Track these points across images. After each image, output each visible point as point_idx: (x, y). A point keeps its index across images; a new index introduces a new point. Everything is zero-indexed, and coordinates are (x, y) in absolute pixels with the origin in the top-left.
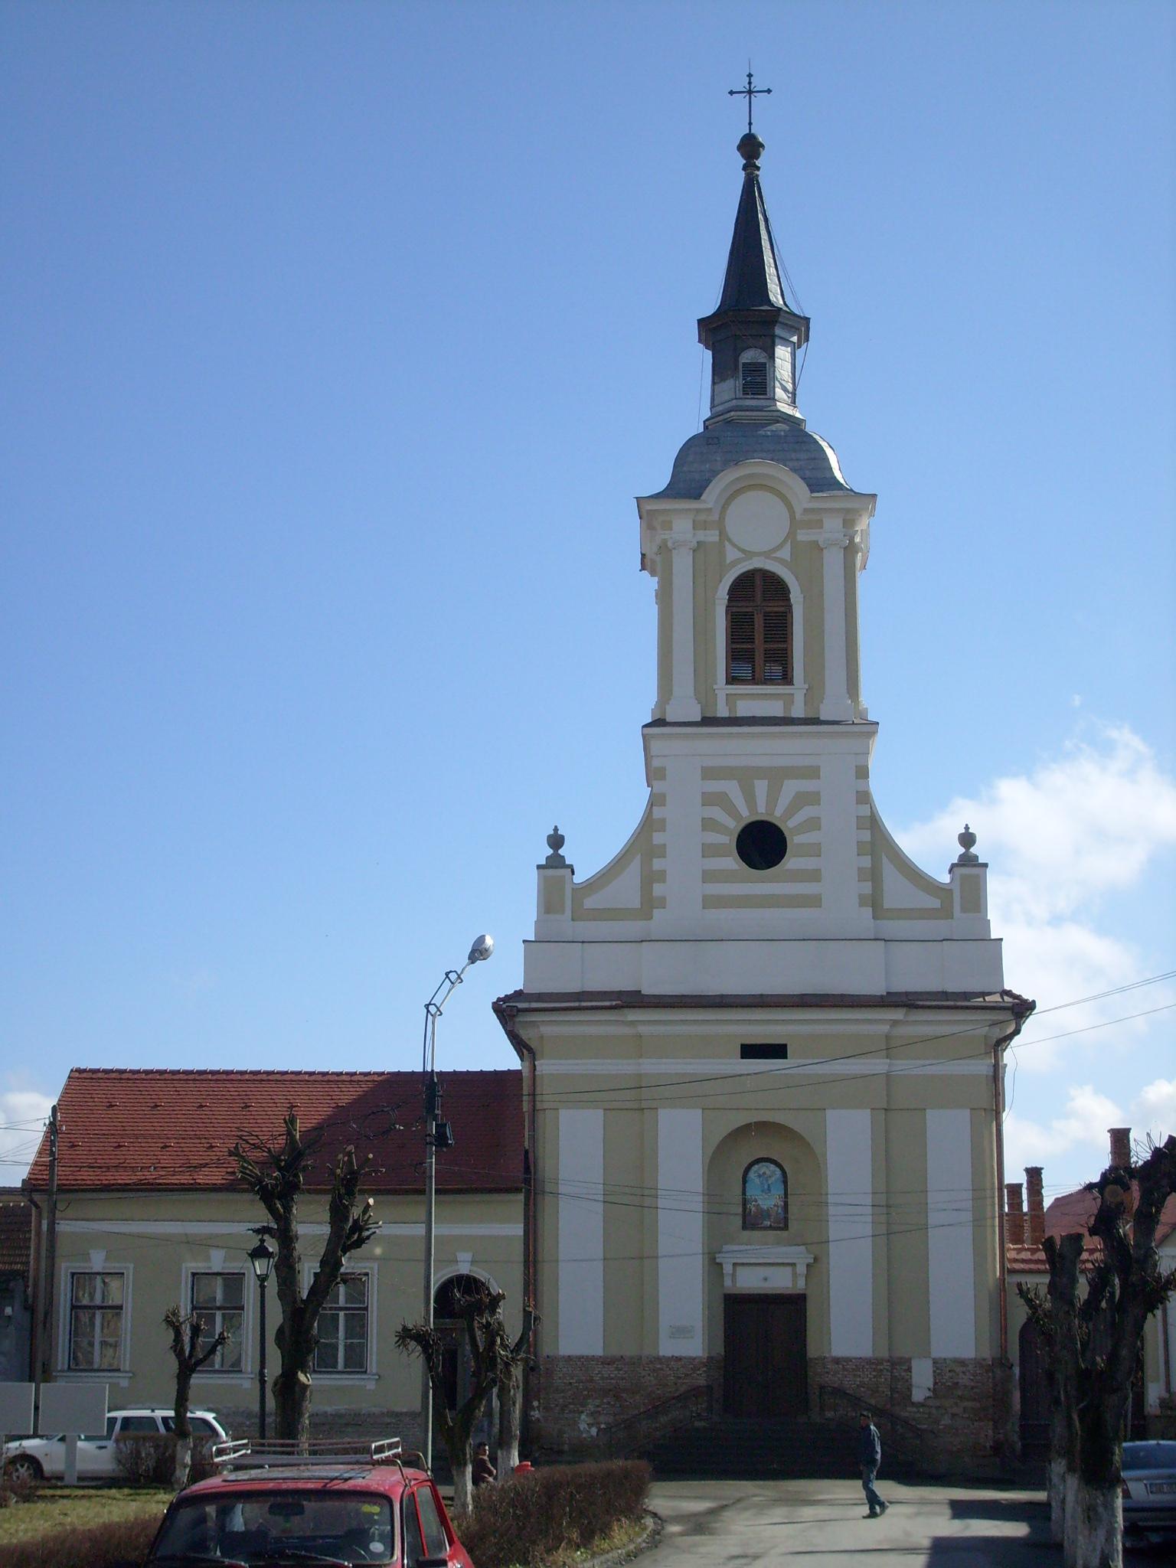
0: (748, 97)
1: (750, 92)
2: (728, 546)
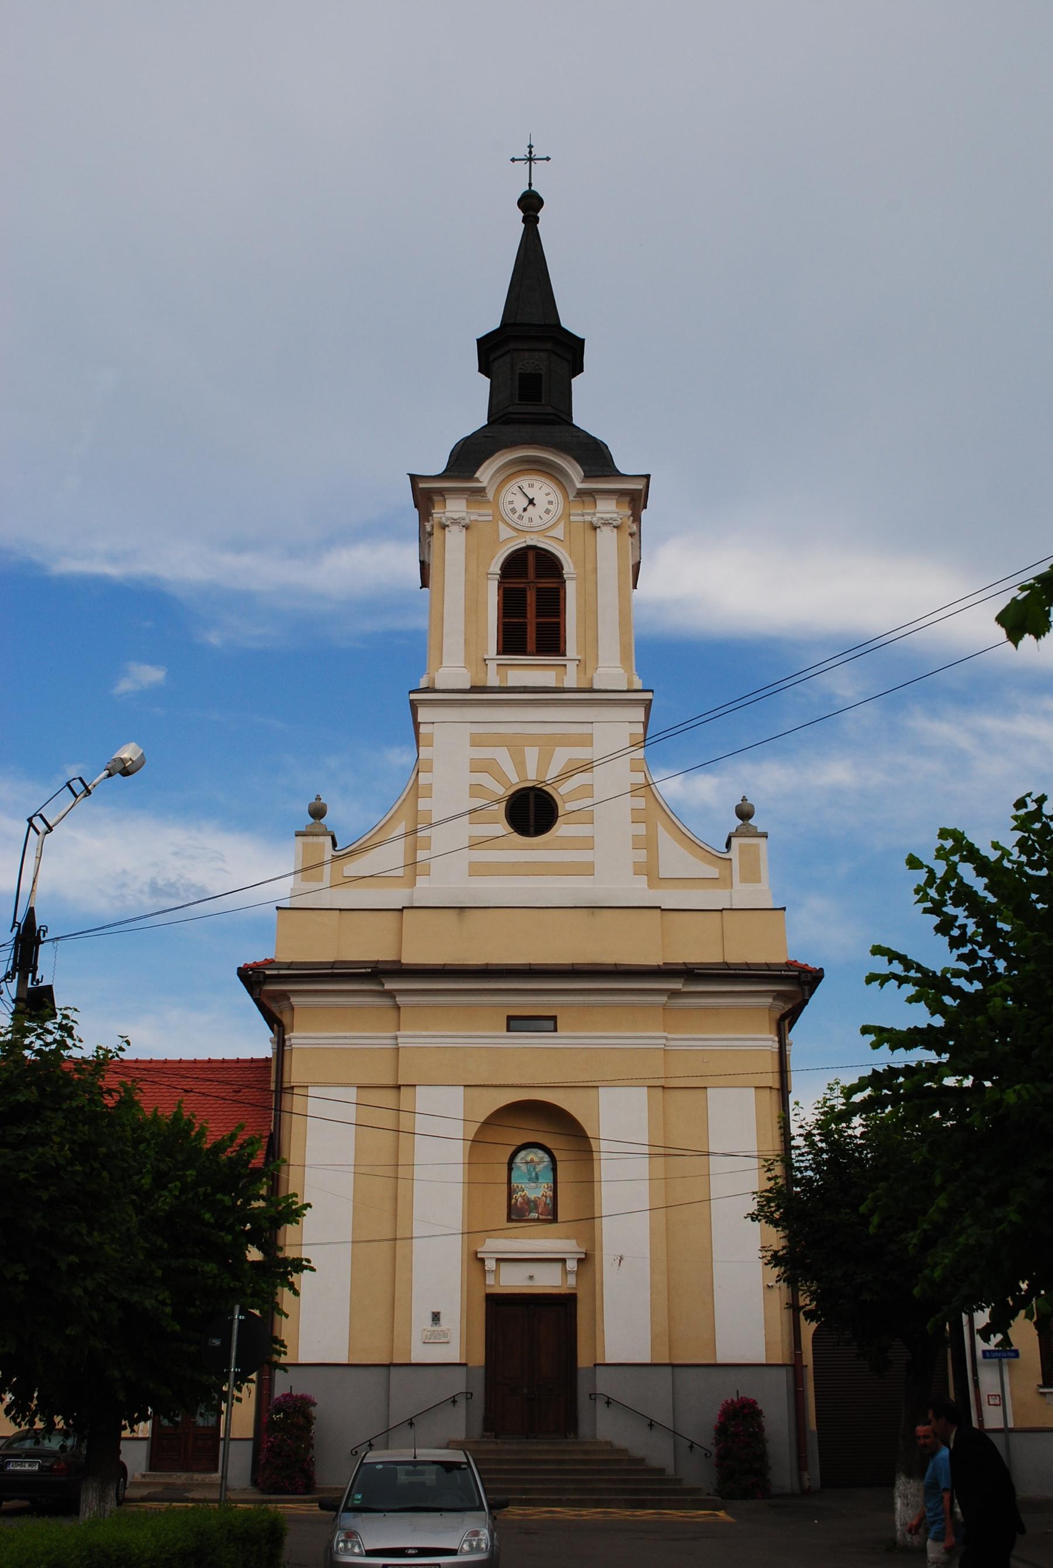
0: (528, 163)
1: (530, 160)
2: (501, 525)
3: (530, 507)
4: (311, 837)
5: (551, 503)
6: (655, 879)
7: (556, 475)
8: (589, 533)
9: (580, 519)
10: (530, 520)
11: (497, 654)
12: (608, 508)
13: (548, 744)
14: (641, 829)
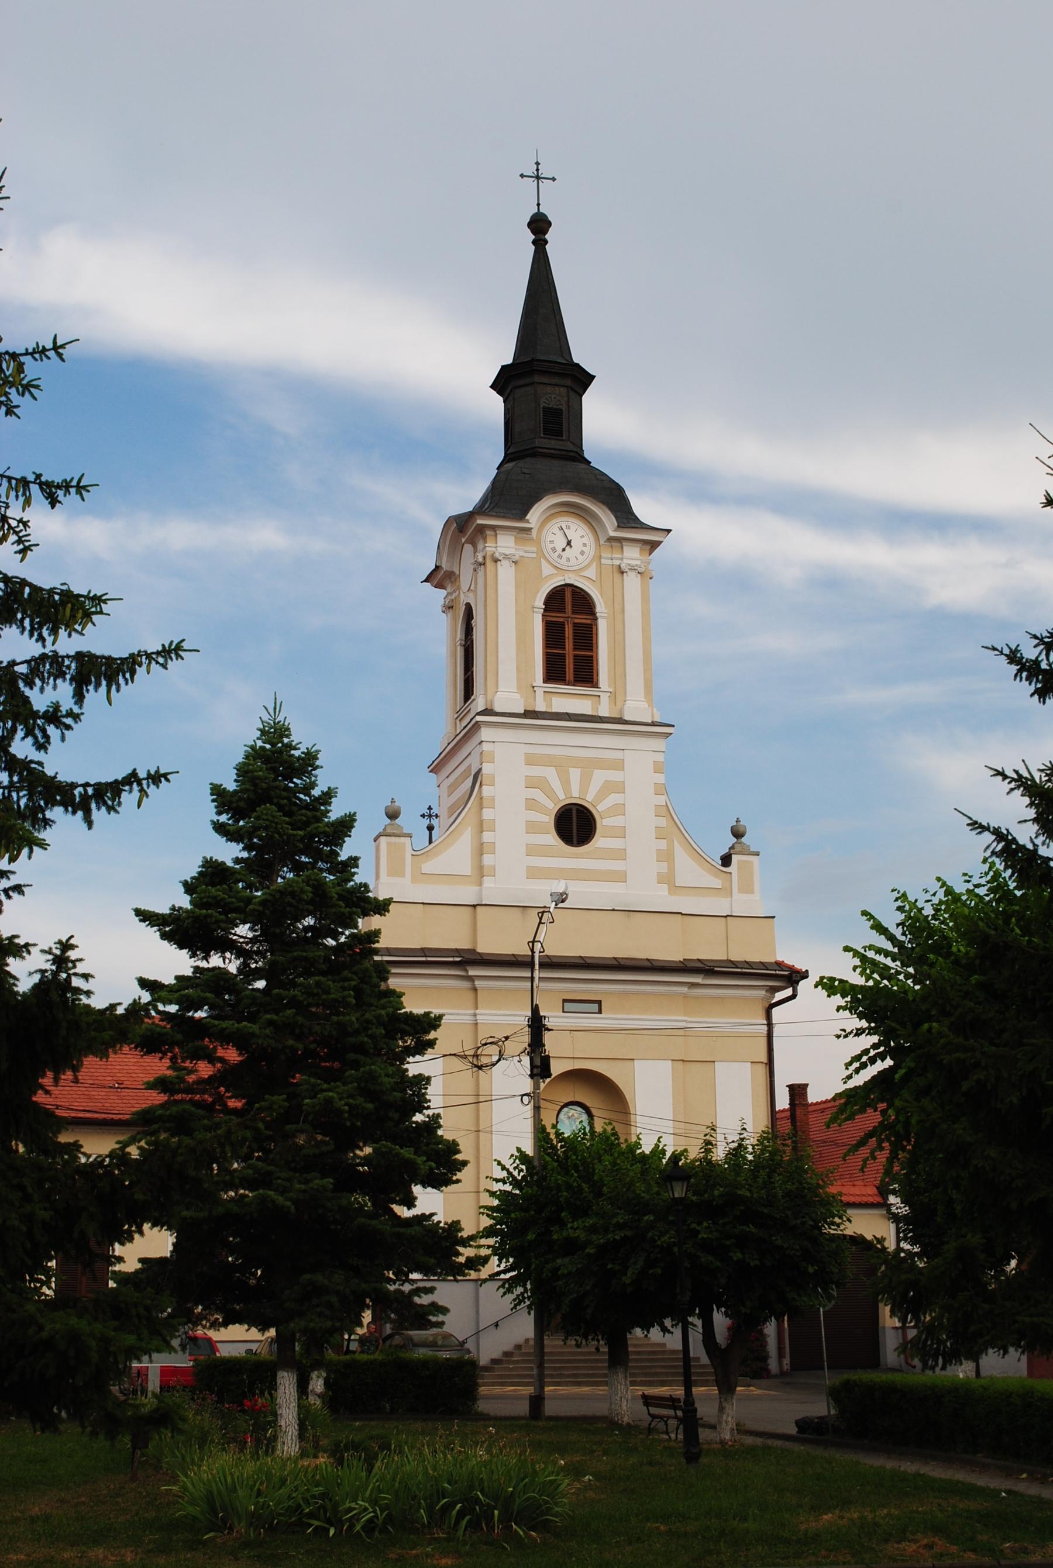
0: (536, 181)
1: (538, 178)
2: (543, 562)
3: (568, 548)
4: (393, 838)
5: (585, 545)
6: (675, 888)
7: (594, 524)
8: (617, 576)
9: (609, 562)
10: (568, 560)
11: (544, 682)
12: (632, 555)
13: (589, 766)
14: (663, 845)
